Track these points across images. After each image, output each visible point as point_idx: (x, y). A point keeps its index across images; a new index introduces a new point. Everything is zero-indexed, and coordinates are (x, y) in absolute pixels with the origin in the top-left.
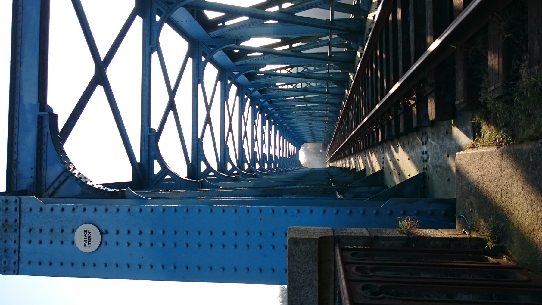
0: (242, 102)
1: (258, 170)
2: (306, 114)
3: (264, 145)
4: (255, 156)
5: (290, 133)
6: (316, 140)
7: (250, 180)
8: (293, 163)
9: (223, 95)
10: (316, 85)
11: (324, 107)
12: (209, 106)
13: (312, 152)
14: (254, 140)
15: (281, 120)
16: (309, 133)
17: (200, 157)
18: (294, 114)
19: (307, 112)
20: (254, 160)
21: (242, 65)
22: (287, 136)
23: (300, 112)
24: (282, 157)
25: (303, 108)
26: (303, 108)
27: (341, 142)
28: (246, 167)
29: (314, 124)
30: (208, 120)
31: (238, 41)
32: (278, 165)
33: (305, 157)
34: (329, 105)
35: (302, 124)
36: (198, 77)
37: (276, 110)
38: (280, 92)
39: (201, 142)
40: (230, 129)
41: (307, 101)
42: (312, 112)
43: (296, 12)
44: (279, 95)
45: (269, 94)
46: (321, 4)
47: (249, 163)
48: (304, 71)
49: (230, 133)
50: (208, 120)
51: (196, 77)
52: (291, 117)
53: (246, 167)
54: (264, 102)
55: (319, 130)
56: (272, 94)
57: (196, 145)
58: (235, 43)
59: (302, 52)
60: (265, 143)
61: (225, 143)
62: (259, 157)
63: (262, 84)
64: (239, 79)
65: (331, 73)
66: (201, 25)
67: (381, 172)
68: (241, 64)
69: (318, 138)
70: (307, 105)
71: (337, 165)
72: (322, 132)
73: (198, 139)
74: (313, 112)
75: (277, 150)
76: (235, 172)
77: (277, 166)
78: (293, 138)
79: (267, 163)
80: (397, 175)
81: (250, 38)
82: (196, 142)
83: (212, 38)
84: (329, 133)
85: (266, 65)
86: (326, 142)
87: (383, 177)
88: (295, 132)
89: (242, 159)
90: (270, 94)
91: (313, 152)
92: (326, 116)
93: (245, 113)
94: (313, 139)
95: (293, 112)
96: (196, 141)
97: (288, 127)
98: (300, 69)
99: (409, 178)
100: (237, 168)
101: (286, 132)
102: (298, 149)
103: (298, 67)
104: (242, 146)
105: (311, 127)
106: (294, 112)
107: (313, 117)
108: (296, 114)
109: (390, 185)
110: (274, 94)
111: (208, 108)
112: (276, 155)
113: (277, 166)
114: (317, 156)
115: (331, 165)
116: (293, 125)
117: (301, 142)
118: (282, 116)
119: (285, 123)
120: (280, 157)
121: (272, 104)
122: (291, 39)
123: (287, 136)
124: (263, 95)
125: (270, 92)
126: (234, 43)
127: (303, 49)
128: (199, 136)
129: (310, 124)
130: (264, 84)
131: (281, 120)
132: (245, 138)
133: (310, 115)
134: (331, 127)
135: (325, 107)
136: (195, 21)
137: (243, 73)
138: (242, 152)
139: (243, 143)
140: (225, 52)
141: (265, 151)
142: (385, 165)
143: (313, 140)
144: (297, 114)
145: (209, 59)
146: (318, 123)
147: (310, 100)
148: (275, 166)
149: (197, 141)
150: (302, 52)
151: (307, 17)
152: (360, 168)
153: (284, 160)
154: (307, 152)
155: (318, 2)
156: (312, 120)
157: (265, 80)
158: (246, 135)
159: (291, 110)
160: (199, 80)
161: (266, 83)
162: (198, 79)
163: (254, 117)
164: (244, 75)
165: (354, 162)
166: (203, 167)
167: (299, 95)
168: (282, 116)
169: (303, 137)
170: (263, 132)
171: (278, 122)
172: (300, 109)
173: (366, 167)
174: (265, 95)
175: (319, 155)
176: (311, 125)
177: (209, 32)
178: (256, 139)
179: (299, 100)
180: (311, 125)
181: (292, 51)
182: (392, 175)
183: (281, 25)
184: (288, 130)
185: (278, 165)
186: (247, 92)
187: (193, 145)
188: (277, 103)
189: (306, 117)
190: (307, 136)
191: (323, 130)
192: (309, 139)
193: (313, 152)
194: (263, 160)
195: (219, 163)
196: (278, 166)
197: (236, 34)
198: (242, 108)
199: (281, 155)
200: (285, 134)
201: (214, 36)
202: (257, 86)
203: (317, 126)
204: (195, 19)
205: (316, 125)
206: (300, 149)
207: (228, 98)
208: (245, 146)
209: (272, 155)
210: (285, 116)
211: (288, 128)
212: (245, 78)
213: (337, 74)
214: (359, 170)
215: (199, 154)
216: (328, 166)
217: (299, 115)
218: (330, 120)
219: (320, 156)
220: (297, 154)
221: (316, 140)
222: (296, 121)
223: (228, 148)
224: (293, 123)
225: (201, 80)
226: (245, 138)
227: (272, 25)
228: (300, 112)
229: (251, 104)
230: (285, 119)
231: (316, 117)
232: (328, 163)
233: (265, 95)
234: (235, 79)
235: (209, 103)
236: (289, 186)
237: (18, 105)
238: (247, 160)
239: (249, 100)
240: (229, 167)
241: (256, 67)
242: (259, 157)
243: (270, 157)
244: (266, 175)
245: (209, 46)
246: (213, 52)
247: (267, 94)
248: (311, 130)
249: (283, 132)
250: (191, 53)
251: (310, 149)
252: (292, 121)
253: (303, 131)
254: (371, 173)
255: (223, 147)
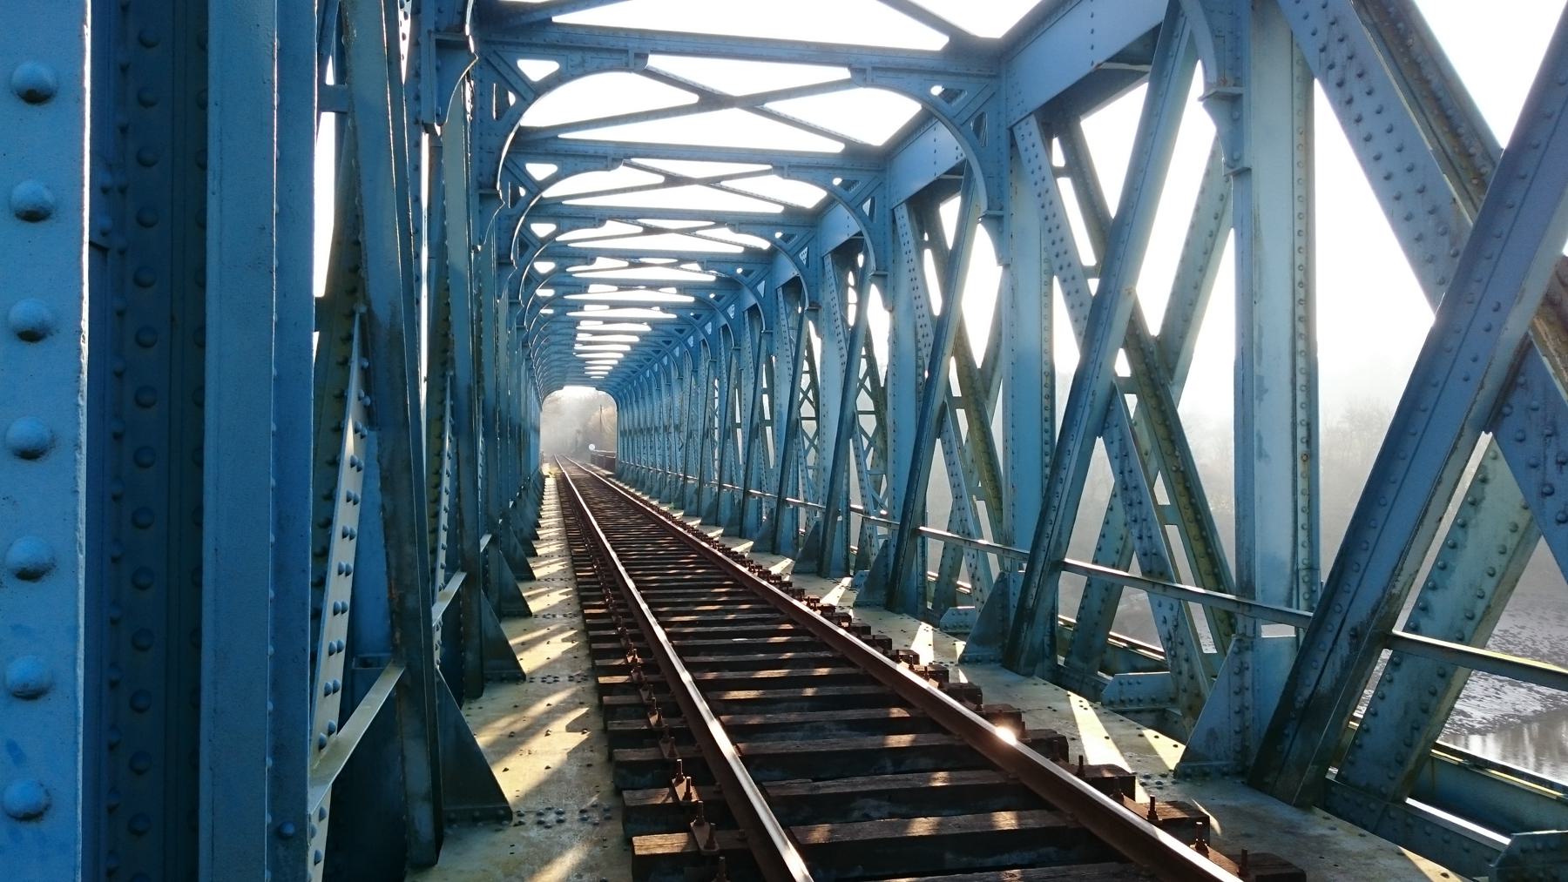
0: (762, 224)
1: (532, 268)
2: (710, 421)
3: (616, 288)
4: (578, 261)
5: (648, 363)
6: (626, 439)
7: (487, 248)
8: (559, 369)
9: (794, 161)
10: (807, 468)
11: (731, 478)
12: (759, 107)
13: (589, 419)
14: (634, 259)
15: (691, 341)
16: (648, 419)
17: (576, 57)
18: (710, 385)
19: (716, 426)
20: (565, 255)
21: (894, 230)
22: (640, 355)
23: (717, 401)
24: (578, 328)
25: (729, 415)
26: (729, 415)
27: (622, 543)
28: (542, 229)
29: (676, 440)
30: (711, 100)
31: (997, 221)
32: (550, 311)
33: (563, 761)
34: (739, 497)
35: (677, 404)
36: (874, 69)
37: (725, 327)
38: (788, 347)
39: (631, 66)
40: (673, 180)
41: (755, 432)
42: (716, 438)
43: (1108, 444)
44: (776, 344)
45: (782, 311)
46: (1140, 538)
47: (558, 239)
48: (863, 437)
49: (661, 179)
50: (711, 100)
51: (876, 59)
52: (703, 371)
53: (542, 229)
54: (756, 294)
55: (657, 451)
56: (784, 323)
57: (621, 45)
58: (991, 213)
59: (938, 441)
60: (620, 290)
61: (626, 161)
62: (577, 237)
63: (821, 291)
64: (842, 213)
65: (848, 518)
66: (1058, 96)
67: (518, 676)
68: (899, 226)
69: (630, 444)
70: (739, 426)
71: (548, 497)
72: (651, 459)
73: (646, 57)
74: (714, 441)
75: (599, 326)
76: (522, 192)
77: (543, 311)
78: (634, 372)
79: (558, 297)
80: (508, 731)
81: (1006, 266)
82: (633, 45)
83: (1011, 130)
84: (648, 483)
85: (891, 311)
86: (618, 467)
87: (480, 824)
88: (653, 379)
89: (569, 217)
90: (783, 316)
91: (590, 423)
92: (701, 482)
93: (724, 233)
94: (630, 431)
95: (716, 381)
96: (636, 46)
97: (669, 358)
98: (869, 424)
99: (518, 658)
100: (535, 197)
101: (654, 354)
102: (600, 385)
103: (874, 416)
104: (612, 218)
105: (666, 428)
106: (716, 384)
107: (698, 440)
108: (710, 389)
109: (471, 714)
110: (783, 329)
111: (754, 103)
112: (587, 307)
113: (543, 311)
114: (579, 432)
115: (550, 483)
116: (674, 375)
117: (620, 394)
118: (705, 344)
119: (683, 354)
120: (576, 321)
121: (747, 320)
122: (983, 405)
123: (640, 355)
124: (780, 293)
125: (788, 316)
126: (989, 208)
127: (951, 447)
128: (655, 61)
129: (677, 428)
130: (820, 299)
131: (691, 341)
132: (640, 229)
133: (707, 434)
134: (666, 492)
135: (731, 483)
136: (1092, 63)
137: (865, 233)
138: (594, 217)
139: (624, 220)
140: (951, 171)
141: (595, 292)
142: (530, 843)
143: (625, 431)
144: (710, 393)
145: (932, 109)
146: (679, 453)
147: (757, 441)
148: (547, 302)
149: (638, 51)
150: (938, 441)
151: (668, 219)
152: (532, 597)
153: (567, 334)
154: (591, 405)
155: (1150, 529)
156: (690, 436)
157: (832, 303)
158: (649, 231)
159: (725, 376)
160: (863, 71)
161: (824, 306)
162: (869, 69)
163: (707, 261)
164: (860, 234)
165: (552, 574)
166: (535, 69)
167: (776, 408)
168: (705, 344)
169: (637, 401)
170: (654, 286)
171: (686, 332)
172: (728, 405)
173: (538, 583)
174: (781, 299)
175: (580, 439)
176: (672, 429)
177: (1035, 115)
178: (633, 265)
179: (758, 405)
180: (672, 429)
181: (943, 408)
182: (514, 713)
183: (1044, 377)
184: (660, 361)
185: (550, 311)
186: (793, 241)
187: (622, 34)
188: (748, 335)
189: (701, 421)
190: (638, 414)
191: (658, 465)
192: (631, 418)
193: (590, 423)
194: (563, 284)
195: (552, 135)
196: (545, 315)
197: (1024, 214)
198: (741, 224)
199: (584, 325)
200: (647, 349)
201: (1018, 134)
202: (813, 270)
203: (669, 448)
204: (1099, 65)
205: (673, 446)
206: (597, 389)
207: (783, 176)
208: (611, 227)
209: (582, 309)
210: (705, 354)
211: (665, 360)
212: (845, 238)
213: (844, 536)
214: (524, 595)
215: (588, 56)
216: (546, 469)
217: (708, 399)
218: (689, 492)
219: (577, 442)
220: (586, 381)
221: (626, 439)
222: (686, 385)
223: (607, 168)
224: (681, 378)
225: (865, 79)
226: (640, 229)
227: (1045, 346)
228: (717, 401)
229: (750, 252)
230: (695, 354)
231: (699, 451)
232: (555, 470)
233: (781, 299)
234: (846, 203)
235: (769, 106)
236: (452, 407)
237: (609, 57)
238: (563, 233)
239: (764, 245)
240: (539, 170)
241: (885, 276)
242: (577, 237)
243: (576, 306)
244: (510, 298)
245: (981, 116)
246: (957, 127)
247: (782, 305)
248: (656, 429)
249: (654, 344)
250: (963, 48)
251: (597, 414)
252: (687, 373)
253: (656, 404)
254: (531, 565)
255: (611, 152)
